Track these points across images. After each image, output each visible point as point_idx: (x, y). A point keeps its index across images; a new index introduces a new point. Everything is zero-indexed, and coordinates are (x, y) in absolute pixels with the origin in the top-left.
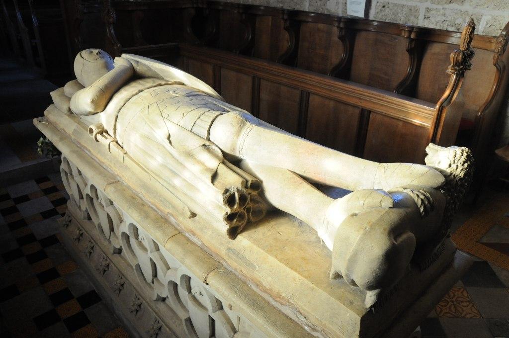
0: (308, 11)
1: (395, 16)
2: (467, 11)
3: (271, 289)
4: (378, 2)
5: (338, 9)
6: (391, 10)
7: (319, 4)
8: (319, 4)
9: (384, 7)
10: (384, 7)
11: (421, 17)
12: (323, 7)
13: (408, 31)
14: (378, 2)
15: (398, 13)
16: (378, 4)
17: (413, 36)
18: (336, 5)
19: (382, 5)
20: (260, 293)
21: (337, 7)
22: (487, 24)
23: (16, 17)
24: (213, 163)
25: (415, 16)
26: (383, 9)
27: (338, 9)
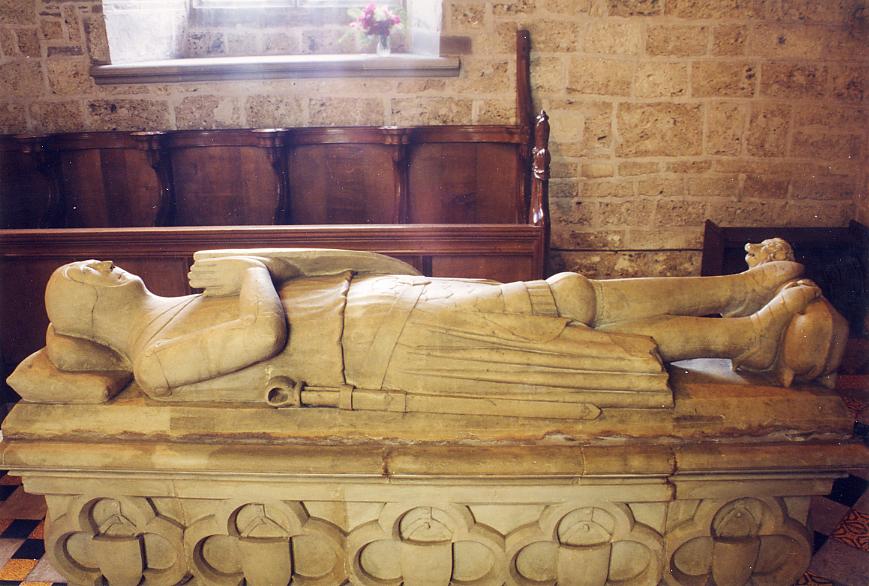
0: (175, 129)
1: (346, 116)
2: (450, 98)
3: (210, 372)
4: (311, 100)
5: (238, 118)
6: (336, 108)
7: (197, 116)
8: (197, 116)
9: (322, 105)
10: (322, 105)
11: (387, 112)
12: (206, 119)
13: (398, 135)
14: (311, 100)
15: (349, 112)
16: (313, 102)
17: (277, 143)
18: (233, 114)
19: (319, 103)
20: (485, 539)
21: (236, 116)
22: (480, 111)
23: (525, 190)
24: (415, 403)
25: (378, 112)
26: (323, 108)
27: (238, 118)
